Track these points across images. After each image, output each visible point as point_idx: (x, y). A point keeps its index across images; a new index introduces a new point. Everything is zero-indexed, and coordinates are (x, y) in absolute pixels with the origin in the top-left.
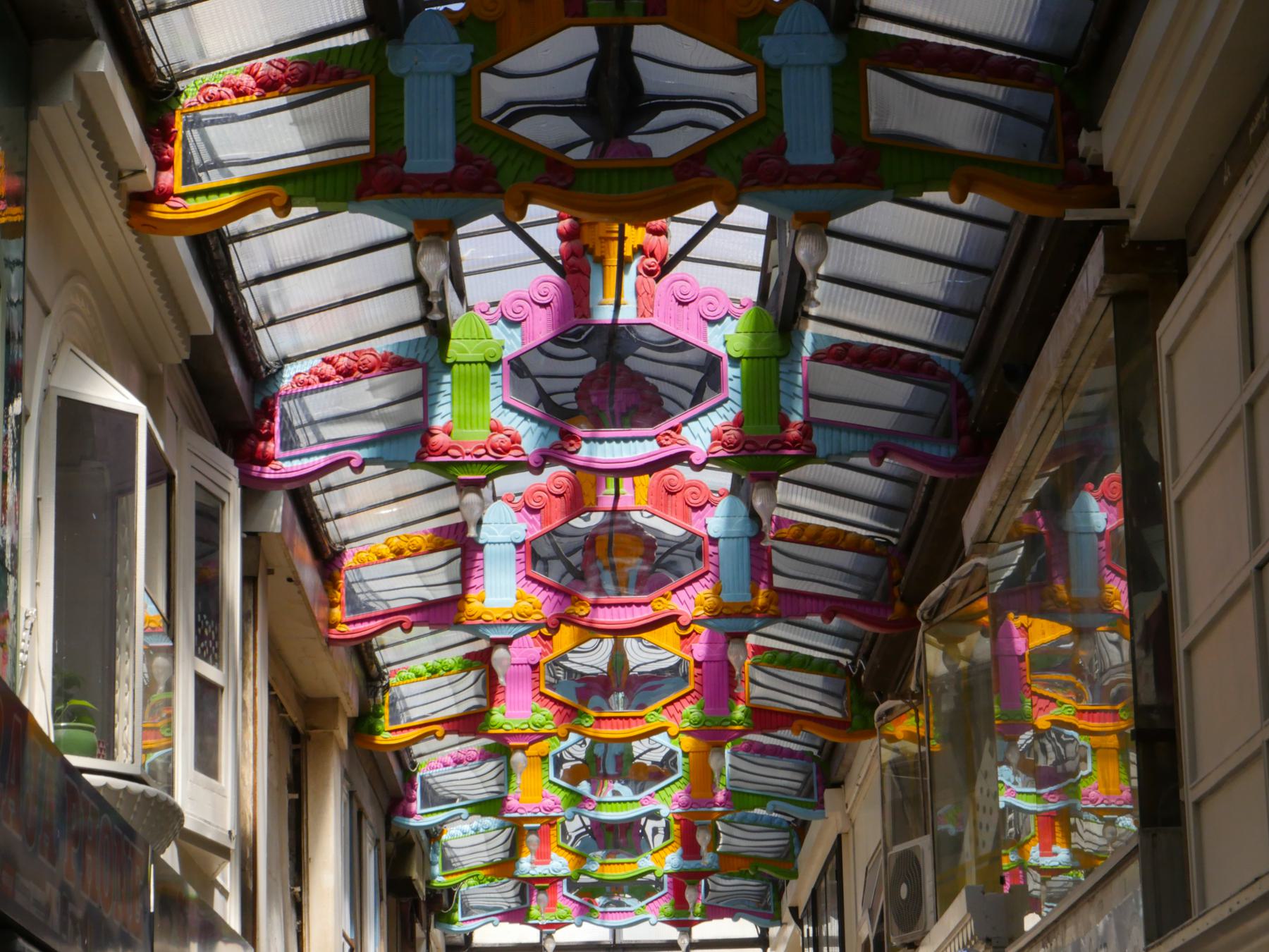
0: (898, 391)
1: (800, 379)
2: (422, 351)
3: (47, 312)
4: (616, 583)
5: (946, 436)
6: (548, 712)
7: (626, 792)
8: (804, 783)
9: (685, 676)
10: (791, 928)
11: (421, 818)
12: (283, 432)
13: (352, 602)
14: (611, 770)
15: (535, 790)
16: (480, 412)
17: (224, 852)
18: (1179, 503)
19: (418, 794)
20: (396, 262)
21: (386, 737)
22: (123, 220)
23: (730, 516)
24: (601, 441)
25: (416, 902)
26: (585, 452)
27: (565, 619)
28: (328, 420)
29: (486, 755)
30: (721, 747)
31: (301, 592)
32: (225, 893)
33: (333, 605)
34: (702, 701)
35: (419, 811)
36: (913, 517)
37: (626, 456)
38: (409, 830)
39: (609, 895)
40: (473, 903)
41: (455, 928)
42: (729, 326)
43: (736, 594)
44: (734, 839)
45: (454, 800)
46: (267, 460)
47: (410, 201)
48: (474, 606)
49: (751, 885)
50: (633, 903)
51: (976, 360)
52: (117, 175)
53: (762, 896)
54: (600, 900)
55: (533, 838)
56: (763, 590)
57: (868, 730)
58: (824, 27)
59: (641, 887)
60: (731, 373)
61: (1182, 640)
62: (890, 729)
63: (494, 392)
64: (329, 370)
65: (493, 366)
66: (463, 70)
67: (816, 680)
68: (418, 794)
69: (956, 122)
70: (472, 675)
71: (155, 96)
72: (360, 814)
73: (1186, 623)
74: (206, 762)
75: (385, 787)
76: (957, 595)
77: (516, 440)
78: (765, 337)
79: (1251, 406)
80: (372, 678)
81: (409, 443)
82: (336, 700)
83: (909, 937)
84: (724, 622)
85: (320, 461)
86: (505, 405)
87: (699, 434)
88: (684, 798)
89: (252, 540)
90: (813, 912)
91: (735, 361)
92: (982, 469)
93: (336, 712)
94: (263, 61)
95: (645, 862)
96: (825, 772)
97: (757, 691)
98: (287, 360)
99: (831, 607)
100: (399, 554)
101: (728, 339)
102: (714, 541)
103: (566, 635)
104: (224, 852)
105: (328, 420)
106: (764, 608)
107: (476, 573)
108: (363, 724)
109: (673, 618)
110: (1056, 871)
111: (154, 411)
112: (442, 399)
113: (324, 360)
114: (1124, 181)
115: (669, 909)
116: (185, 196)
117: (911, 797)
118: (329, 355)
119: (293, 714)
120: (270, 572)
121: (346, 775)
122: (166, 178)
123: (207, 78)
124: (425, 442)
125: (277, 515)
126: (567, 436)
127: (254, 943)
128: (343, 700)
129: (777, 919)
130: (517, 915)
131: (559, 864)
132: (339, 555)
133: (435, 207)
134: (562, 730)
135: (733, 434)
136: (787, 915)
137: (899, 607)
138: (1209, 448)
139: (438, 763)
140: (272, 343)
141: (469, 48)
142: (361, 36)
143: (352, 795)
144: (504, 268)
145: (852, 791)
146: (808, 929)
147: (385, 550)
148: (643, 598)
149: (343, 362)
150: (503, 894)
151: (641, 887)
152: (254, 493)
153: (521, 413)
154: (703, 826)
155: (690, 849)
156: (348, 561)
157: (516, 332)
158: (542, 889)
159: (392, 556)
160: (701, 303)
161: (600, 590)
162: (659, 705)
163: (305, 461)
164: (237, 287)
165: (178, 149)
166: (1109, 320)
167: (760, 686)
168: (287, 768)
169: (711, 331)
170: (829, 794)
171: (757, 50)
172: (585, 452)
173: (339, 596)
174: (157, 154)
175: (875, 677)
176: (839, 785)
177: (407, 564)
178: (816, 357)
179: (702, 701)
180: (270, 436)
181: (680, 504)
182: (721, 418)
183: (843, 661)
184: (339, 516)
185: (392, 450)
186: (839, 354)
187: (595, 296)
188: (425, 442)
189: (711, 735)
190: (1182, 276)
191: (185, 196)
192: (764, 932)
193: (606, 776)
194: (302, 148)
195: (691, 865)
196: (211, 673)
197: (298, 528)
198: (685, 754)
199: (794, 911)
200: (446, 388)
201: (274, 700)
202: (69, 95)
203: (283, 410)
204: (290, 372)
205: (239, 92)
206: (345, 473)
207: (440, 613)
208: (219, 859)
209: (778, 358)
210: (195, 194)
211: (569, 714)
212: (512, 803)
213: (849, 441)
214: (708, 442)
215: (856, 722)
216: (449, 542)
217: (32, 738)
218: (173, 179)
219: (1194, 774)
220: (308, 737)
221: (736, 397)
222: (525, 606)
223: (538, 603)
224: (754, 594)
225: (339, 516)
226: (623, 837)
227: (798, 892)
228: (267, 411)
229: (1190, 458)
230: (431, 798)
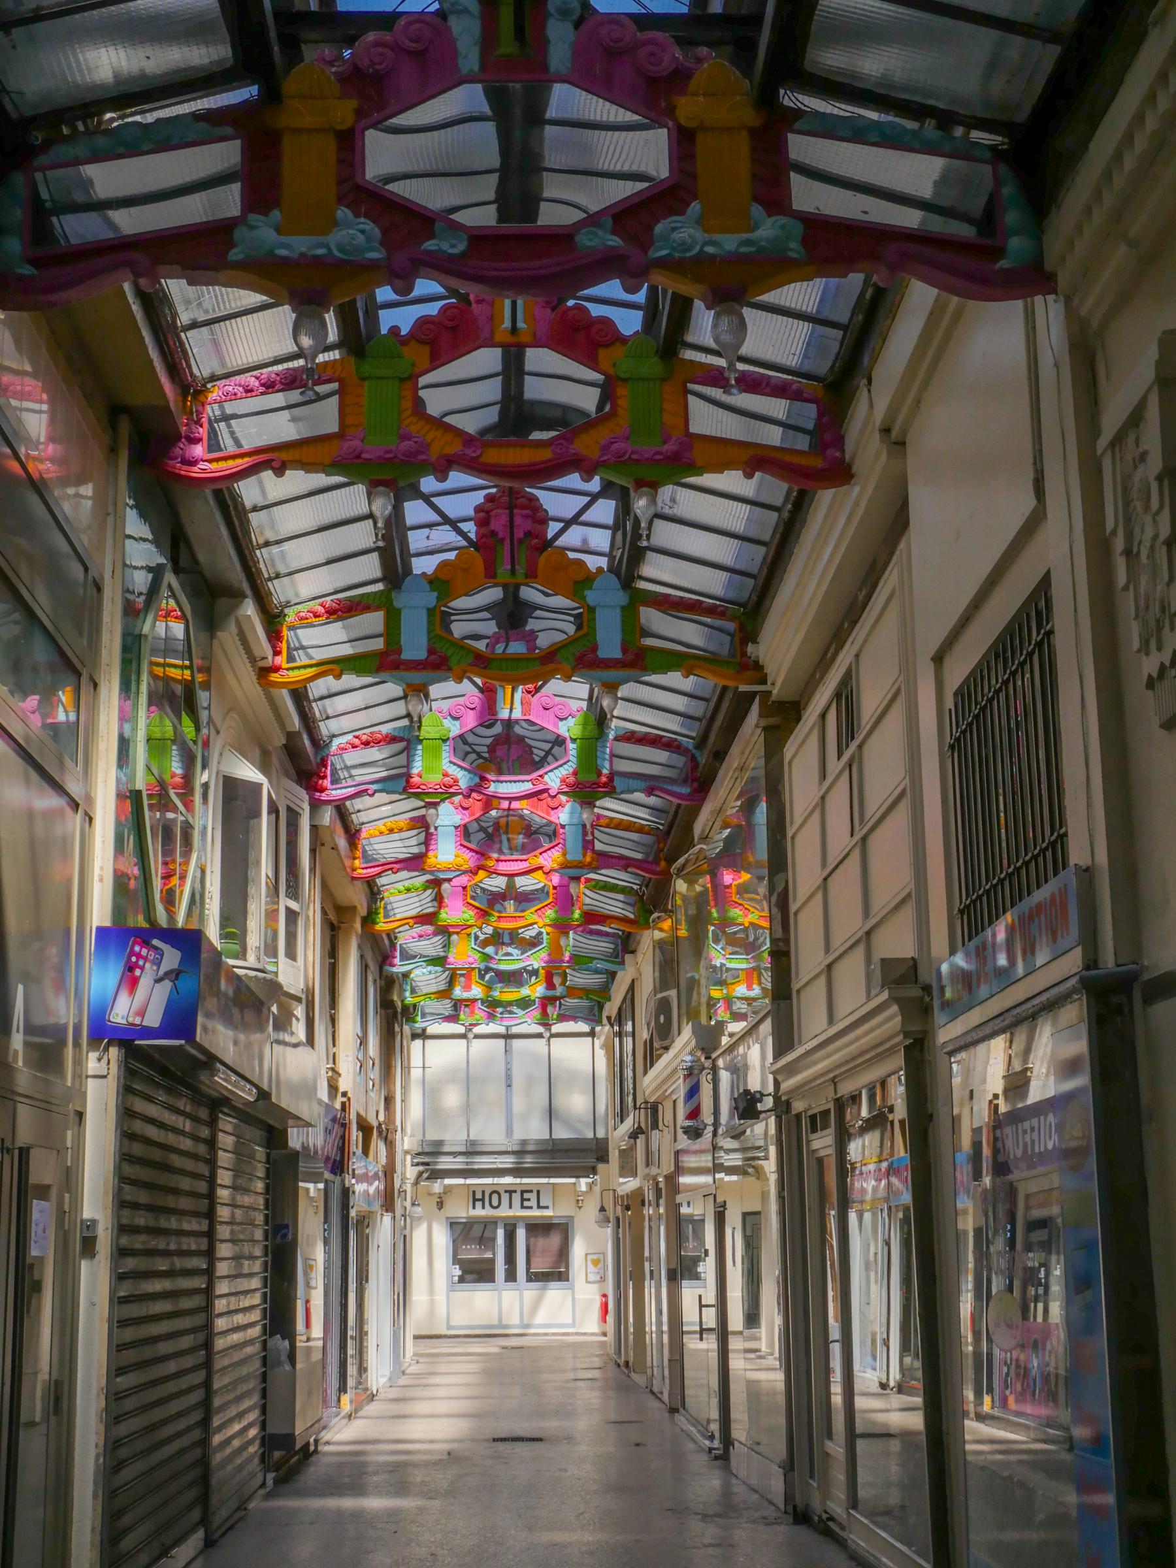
0: (662, 756)
1: (608, 750)
2: (407, 733)
3: (218, 732)
4: (511, 849)
5: (685, 781)
6: (472, 913)
7: (515, 952)
8: (614, 949)
9: (548, 893)
10: (607, 1028)
11: (399, 967)
12: (332, 775)
13: (366, 857)
14: (506, 939)
15: (464, 953)
16: (436, 766)
17: (299, 1000)
18: (793, 838)
19: (398, 954)
20: (400, 708)
21: (381, 926)
22: (255, 681)
23: (572, 813)
24: (502, 782)
25: (396, 1013)
26: (493, 788)
27: (480, 868)
28: (355, 767)
29: (435, 934)
30: (567, 933)
31: (339, 854)
32: (298, 1019)
33: (355, 858)
34: (556, 908)
35: (285, 665)
36: (670, 818)
37: (515, 790)
38: (392, 973)
39: (505, 1007)
40: (427, 1011)
41: (417, 1025)
42: (571, 722)
43: (575, 855)
44: (577, 978)
45: (415, 957)
46: (323, 790)
47: (403, 673)
48: (431, 860)
49: (585, 1003)
50: (520, 1012)
51: (701, 743)
52: (253, 659)
53: (591, 1009)
54: (500, 1010)
55: (462, 979)
56: (589, 854)
57: (647, 926)
58: (619, 586)
59: (524, 1003)
60: (571, 746)
61: (793, 908)
62: (660, 925)
63: (445, 755)
64: (357, 741)
65: (445, 741)
66: (431, 606)
67: (621, 897)
68: (398, 954)
69: (689, 633)
70: (429, 892)
71: (273, 620)
72: (366, 966)
73: (795, 900)
74: (291, 954)
75: (380, 951)
76: (692, 863)
77: (456, 781)
78: (589, 728)
79: (823, 798)
80: (374, 893)
81: (401, 782)
82: (355, 907)
83: (665, 1043)
84: (567, 871)
85: (351, 791)
86: (451, 762)
87: (554, 779)
88: (546, 958)
89: (314, 828)
90: (620, 1019)
91: (574, 740)
92: (704, 799)
93: (355, 915)
94: (329, 599)
95: (525, 991)
96: (625, 946)
97: (588, 901)
98: (334, 736)
99: (625, 863)
100: (391, 831)
101: (569, 728)
102: (563, 827)
103: (482, 873)
104: (299, 1000)
105: (355, 767)
106: (590, 864)
107: (433, 842)
108: (369, 920)
109: (541, 868)
110: (754, 999)
111: (270, 782)
112: (417, 758)
113: (356, 737)
114: (770, 669)
115: (539, 1016)
116: (288, 669)
117: (669, 965)
118: (357, 733)
119: (332, 917)
120: (323, 845)
121: (360, 947)
122: (278, 659)
123: (299, 607)
124: (408, 781)
125: (327, 816)
126: (483, 779)
127: (313, 1047)
128: (359, 907)
129: (599, 1022)
130: (453, 1018)
131: (477, 991)
132: (358, 831)
133: (417, 677)
134: (479, 923)
135: (572, 779)
136: (605, 1021)
137: (663, 864)
138: (890, 696)
139: (408, 938)
140: (325, 728)
141: (435, 594)
142: (380, 586)
143: (362, 956)
144: (450, 704)
145: (640, 956)
146: (616, 1028)
147: (383, 829)
148: (524, 857)
149: (364, 738)
150: (445, 1007)
151: (524, 1003)
152: (316, 805)
153: (459, 766)
154: (557, 974)
155: (550, 985)
156: (363, 835)
157: (457, 723)
158: (466, 1006)
159: (262, 389)
160: (556, 708)
161: (500, 852)
162: (533, 910)
163: (344, 791)
164: (309, 701)
165: (284, 645)
166: (762, 738)
167: (587, 898)
168: (328, 946)
169: (561, 724)
170: (628, 957)
171: (584, 598)
172: (493, 788)
173: (358, 854)
174: (274, 647)
175: (652, 899)
176: (633, 952)
177: (396, 836)
178: (616, 739)
179: (556, 908)
180: (325, 777)
181: (545, 806)
182: (566, 771)
183: (635, 887)
184: (359, 811)
185: (389, 785)
186: (630, 737)
187: (499, 704)
188: (408, 781)
189: (561, 927)
190: (799, 719)
191: (288, 669)
192: (593, 1030)
193: (503, 944)
194: (284, 404)
195: (551, 993)
196: (294, 905)
197: (338, 822)
198: (548, 934)
199: (609, 1018)
200: (419, 752)
201: (324, 912)
202: (233, 628)
203: (332, 764)
204: (336, 742)
205: (316, 616)
206: (407, 927)
207: (415, 862)
208: (295, 1003)
209: (597, 739)
210: (293, 669)
211: (483, 914)
212: (451, 959)
213: (634, 783)
214: (558, 783)
215: (642, 921)
216: (419, 825)
217: (204, 947)
218: (281, 660)
219: (797, 974)
220: (340, 928)
221: (574, 759)
222: (459, 860)
223: (467, 859)
224: (584, 856)
225: (359, 811)
226: (513, 978)
227: (611, 1008)
228: (323, 763)
229: (798, 820)
230: (407, 956)
